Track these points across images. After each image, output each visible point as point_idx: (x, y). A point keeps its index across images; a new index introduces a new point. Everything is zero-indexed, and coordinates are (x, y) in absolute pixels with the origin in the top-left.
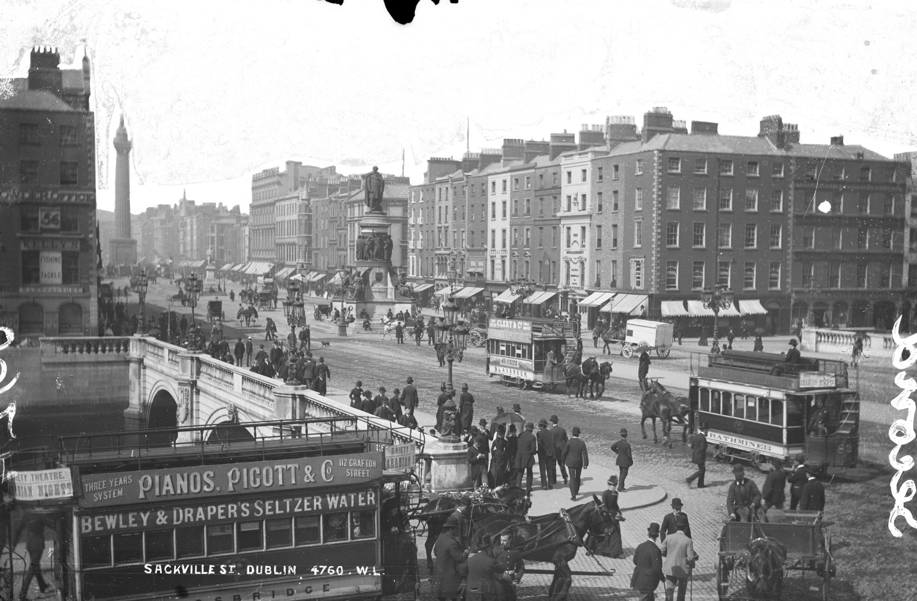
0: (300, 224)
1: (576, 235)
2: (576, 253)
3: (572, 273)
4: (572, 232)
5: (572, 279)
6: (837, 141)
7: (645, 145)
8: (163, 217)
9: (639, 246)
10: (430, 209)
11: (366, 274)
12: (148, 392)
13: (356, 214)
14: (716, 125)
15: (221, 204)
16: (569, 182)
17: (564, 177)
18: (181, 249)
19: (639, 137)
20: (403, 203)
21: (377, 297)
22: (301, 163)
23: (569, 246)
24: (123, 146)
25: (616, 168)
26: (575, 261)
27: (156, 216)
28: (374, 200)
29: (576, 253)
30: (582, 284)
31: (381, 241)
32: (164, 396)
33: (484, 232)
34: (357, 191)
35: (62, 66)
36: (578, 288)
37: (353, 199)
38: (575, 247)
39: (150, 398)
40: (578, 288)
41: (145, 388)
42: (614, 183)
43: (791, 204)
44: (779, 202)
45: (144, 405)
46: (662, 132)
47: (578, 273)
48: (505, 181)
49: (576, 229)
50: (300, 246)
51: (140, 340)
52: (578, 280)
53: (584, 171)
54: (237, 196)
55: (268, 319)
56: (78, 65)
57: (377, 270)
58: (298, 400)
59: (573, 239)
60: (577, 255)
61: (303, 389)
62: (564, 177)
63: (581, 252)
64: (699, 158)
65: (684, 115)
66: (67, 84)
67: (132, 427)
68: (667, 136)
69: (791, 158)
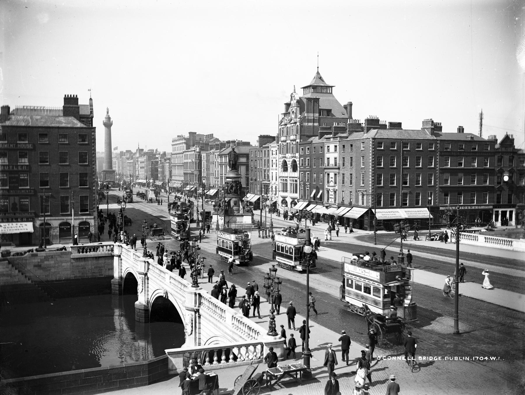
0: (196, 164)
1: (332, 178)
2: (332, 186)
3: (330, 196)
4: (330, 176)
6: (461, 130)
7: (365, 135)
8: (128, 156)
9: (363, 185)
11: (229, 202)
12: (123, 272)
13: (224, 161)
14: (401, 123)
15: (157, 150)
17: (326, 148)
18: (137, 173)
19: (362, 129)
20: (247, 156)
21: (236, 213)
24: (108, 125)
25: (352, 145)
27: (125, 155)
28: (233, 164)
29: (332, 186)
30: (335, 200)
31: (236, 186)
32: (130, 275)
34: (224, 149)
35: (80, 103)
36: (333, 204)
37: (223, 153)
38: (332, 184)
39: (124, 275)
40: (333, 204)
41: (121, 269)
42: (351, 153)
43: (437, 183)
44: (432, 162)
45: (121, 278)
46: (374, 128)
49: (332, 175)
50: (196, 175)
51: (119, 246)
52: (333, 200)
53: (336, 146)
55: (183, 277)
56: (87, 103)
57: (234, 199)
58: (198, 295)
59: (330, 179)
60: (333, 188)
62: (326, 148)
64: (392, 142)
65: (385, 119)
66: (82, 112)
67: (115, 288)
68: (376, 130)
69: (438, 140)
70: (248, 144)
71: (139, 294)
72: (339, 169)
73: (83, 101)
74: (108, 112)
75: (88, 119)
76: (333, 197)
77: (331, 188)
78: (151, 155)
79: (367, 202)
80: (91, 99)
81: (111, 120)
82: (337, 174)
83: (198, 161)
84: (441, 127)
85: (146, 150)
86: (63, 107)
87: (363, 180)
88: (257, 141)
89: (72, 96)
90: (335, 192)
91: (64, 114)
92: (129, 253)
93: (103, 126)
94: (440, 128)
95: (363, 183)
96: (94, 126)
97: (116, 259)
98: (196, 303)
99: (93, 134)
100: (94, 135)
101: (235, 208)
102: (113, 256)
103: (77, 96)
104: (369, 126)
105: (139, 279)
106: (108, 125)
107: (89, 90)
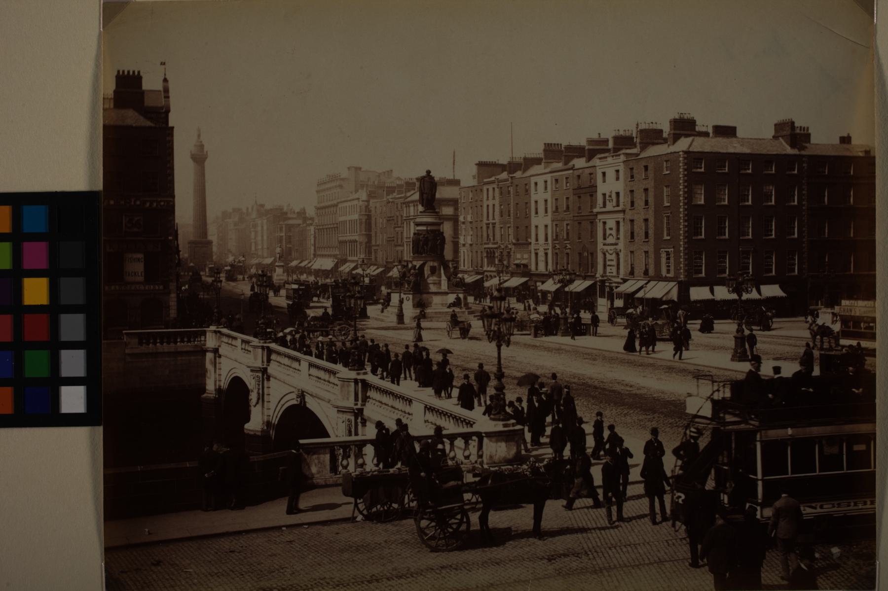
1: (611, 229)
2: (612, 244)
3: (608, 263)
4: (608, 227)
6: (846, 140)
9: (669, 238)
12: (223, 378)
18: (253, 248)
19: (665, 141)
20: (454, 203)
21: (433, 289)
29: (612, 244)
34: (412, 192)
35: (146, 86)
36: (614, 277)
39: (224, 384)
40: (614, 277)
45: (219, 390)
46: (687, 136)
49: (611, 224)
50: (361, 243)
51: (215, 332)
52: (614, 269)
53: (617, 171)
56: (159, 87)
58: (360, 384)
59: (608, 232)
60: (612, 247)
66: (149, 102)
70: (455, 182)
71: (252, 408)
72: (624, 211)
73: (151, 83)
74: (199, 136)
75: (160, 115)
76: (614, 263)
77: (609, 248)
78: (279, 216)
79: (677, 269)
80: (165, 80)
81: (205, 150)
82: (621, 221)
83: (364, 218)
84: (809, 135)
85: (268, 206)
86: (115, 92)
87: (668, 229)
88: (474, 177)
89: (131, 73)
90: (618, 254)
91: (115, 105)
92: (234, 342)
93: (191, 162)
94: (807, 137)
95: (668, 235)
96: (171, 124)
97: (209, 356)
98: (356, 399)
99: (168, 138)
100: (172, 142)
101: (431, 280)
102: (206, 351)
103: (139, 72)
104: (678, 132)
105: (251, 382)
106: (199, 159)
107: (163, 64)
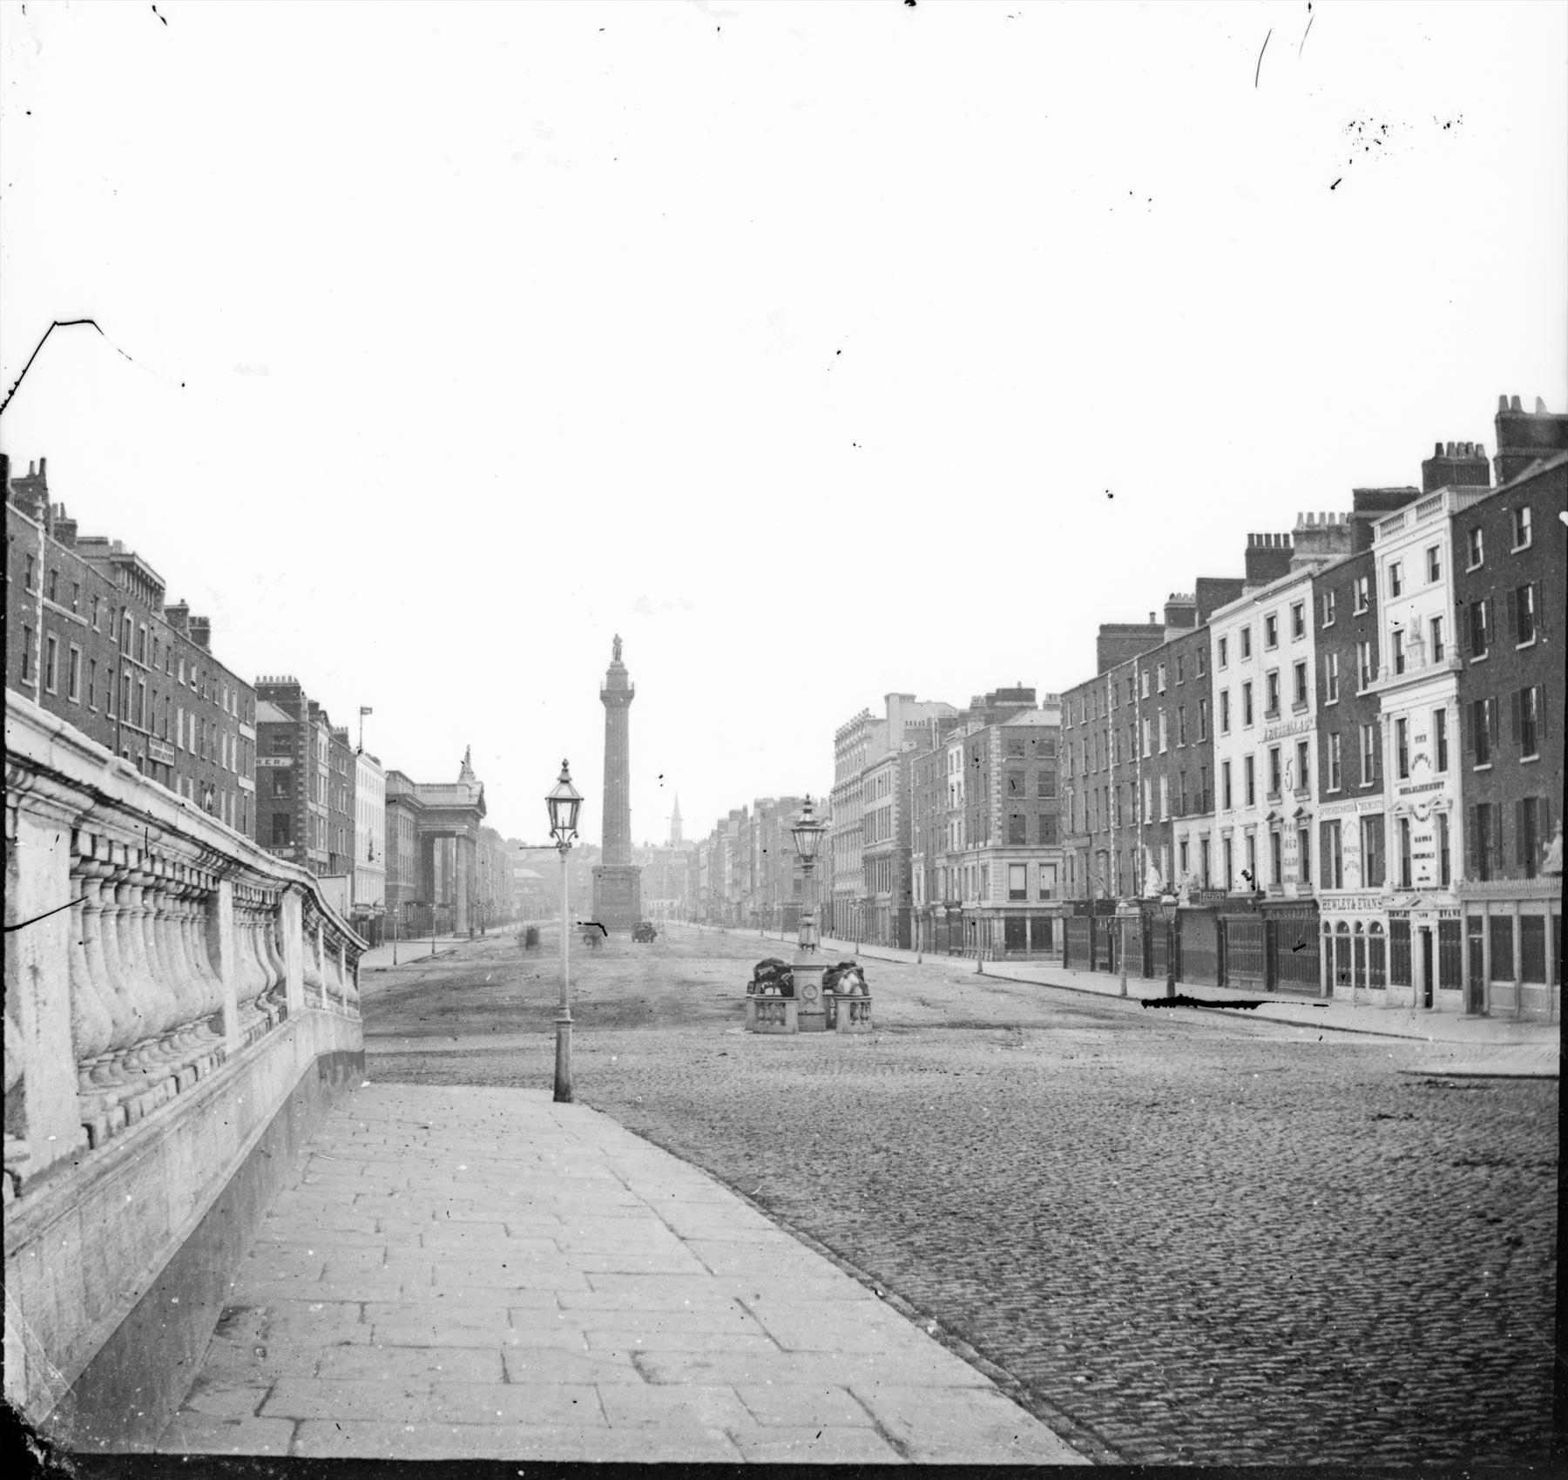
2: (1424, 788)
3: (1416, 848)
5: (1416, 866)
10: (1102, 736)
16: (1396, 592)
22: (912, 697)
23: (1404, 775)
26: (1422, 813)
29: (1424, 788)
33: (1207, 769)
47: (1432, 847)
48: (1246, 632)
54: (815, 778)
59: (1414, 750)
61: (1160, 1104)
63: (1438, 785)
